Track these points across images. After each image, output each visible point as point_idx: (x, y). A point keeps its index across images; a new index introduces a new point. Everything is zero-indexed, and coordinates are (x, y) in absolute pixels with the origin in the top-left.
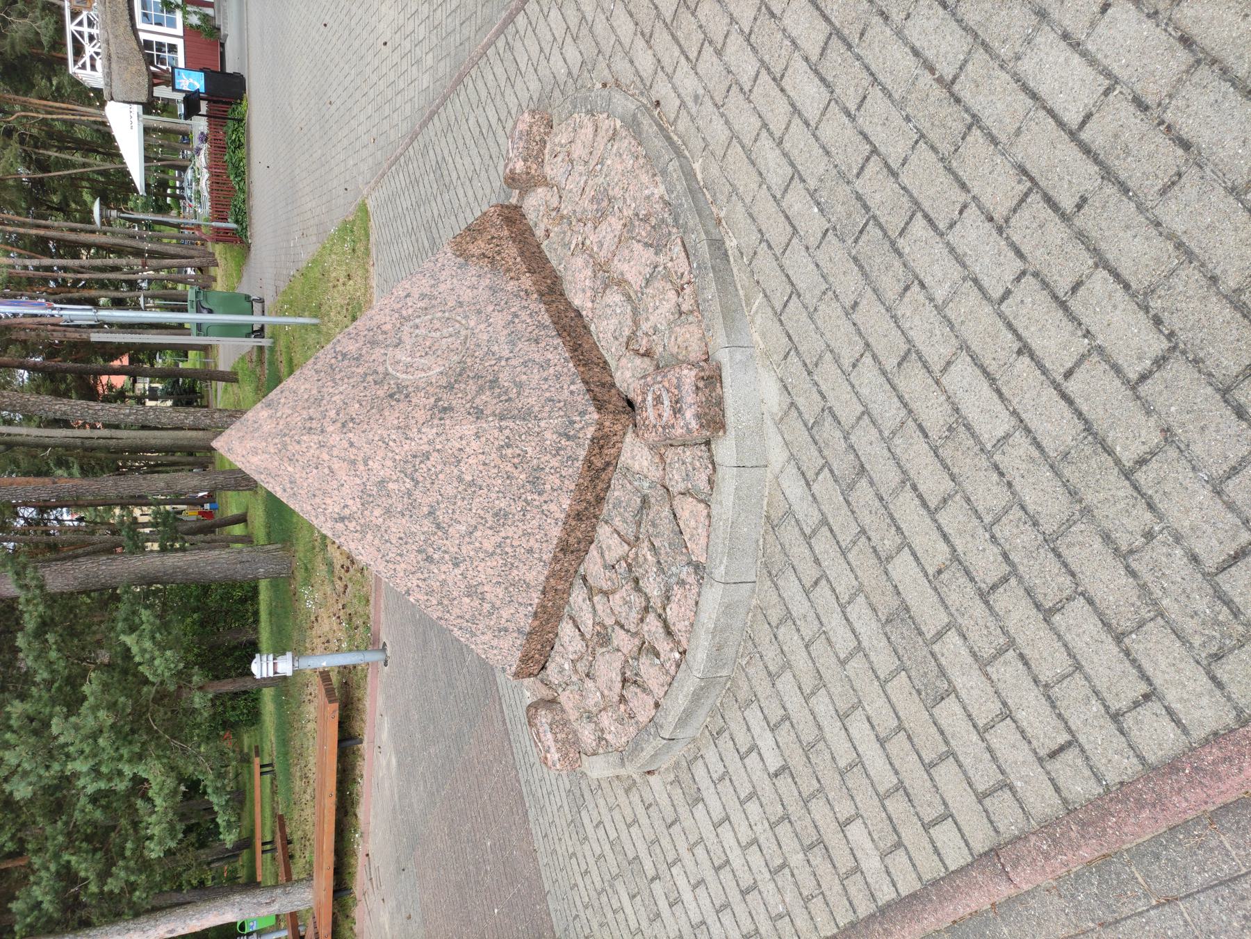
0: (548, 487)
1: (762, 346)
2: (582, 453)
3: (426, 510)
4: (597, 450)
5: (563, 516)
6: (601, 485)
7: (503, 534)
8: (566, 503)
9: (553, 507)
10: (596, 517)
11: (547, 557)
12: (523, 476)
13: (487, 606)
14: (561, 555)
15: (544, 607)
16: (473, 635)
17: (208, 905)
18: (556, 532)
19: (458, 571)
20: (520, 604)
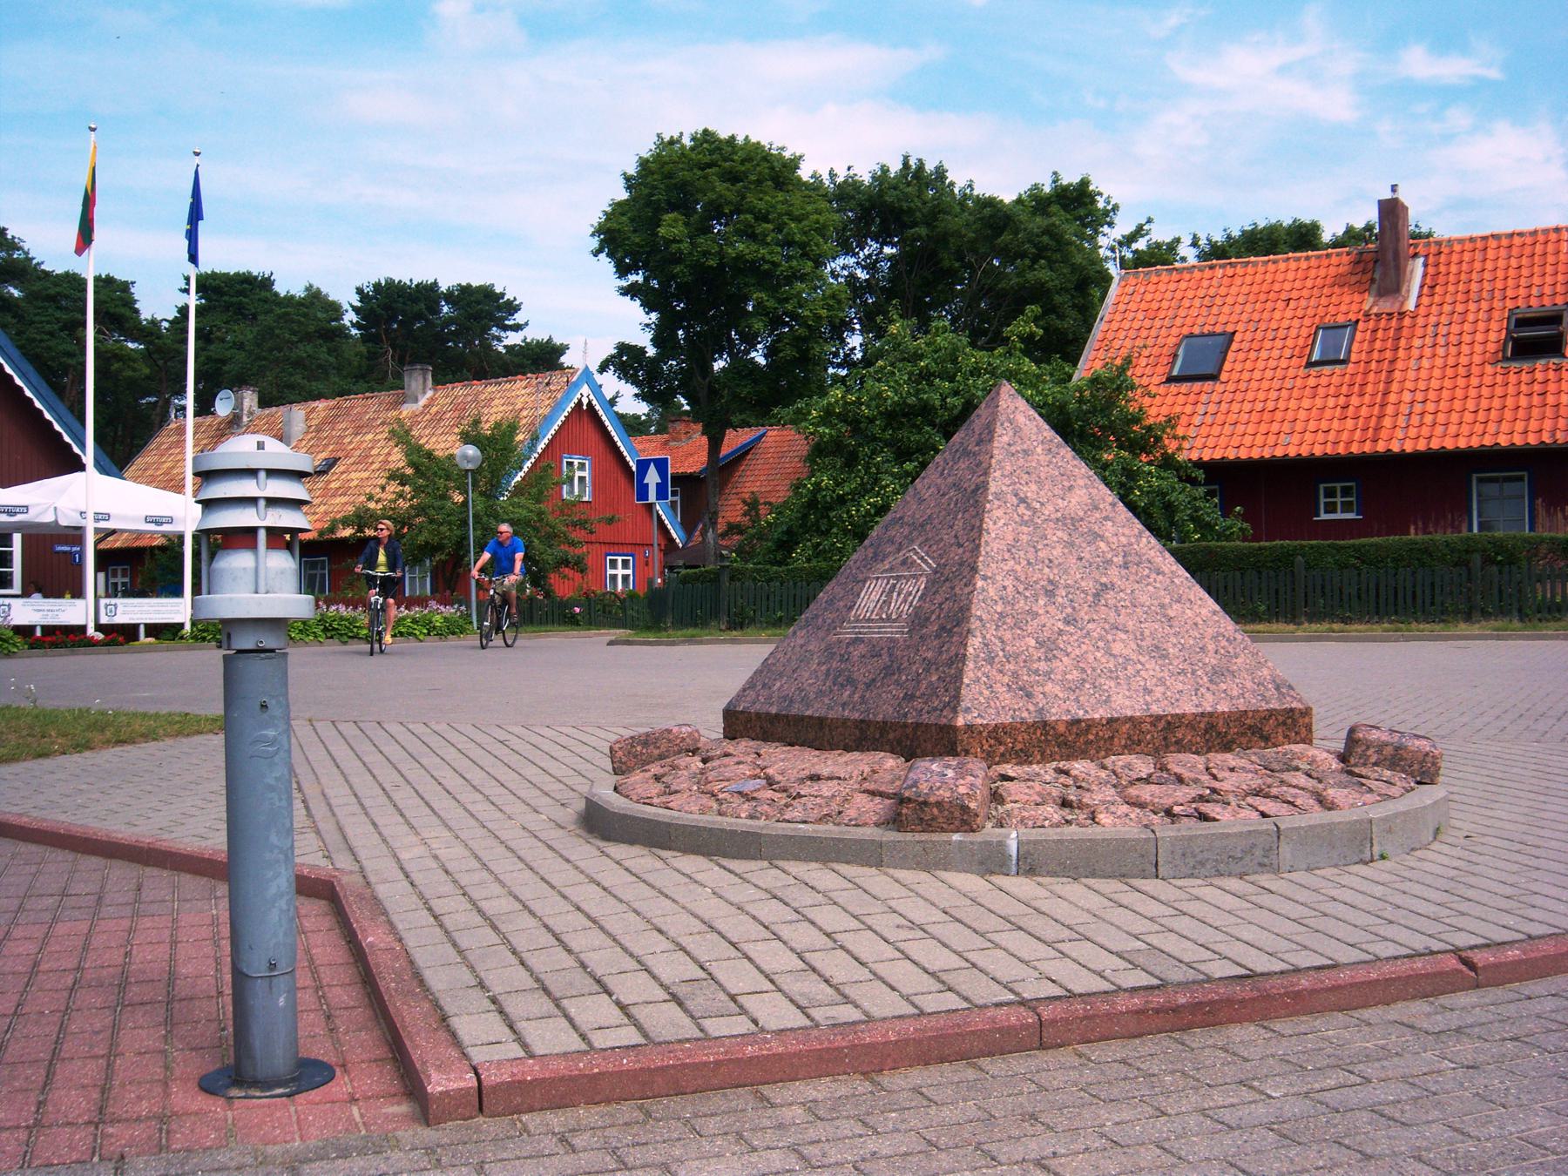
0: (1223, 686)
1: (1411, 305)
2: (1274, 705)
3: (1104, 580)
4: (1281, 719)
5: (1209, 709)
6: (1244, 740)
7: (1142, 659)
8: (1223, 707)
9: (1208, 695)
10: (1209, 750)
11: (1156, 709)
12: (1214, 662)
13: (1043, 666)
14: (1161, 725)
15: (1089, 727)
16: (991, 660)
17: (1378, 629)
18: (1188, 707)
19: (1060, 625)
20: (1077, 700)
